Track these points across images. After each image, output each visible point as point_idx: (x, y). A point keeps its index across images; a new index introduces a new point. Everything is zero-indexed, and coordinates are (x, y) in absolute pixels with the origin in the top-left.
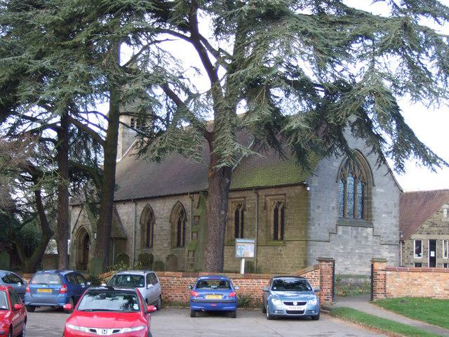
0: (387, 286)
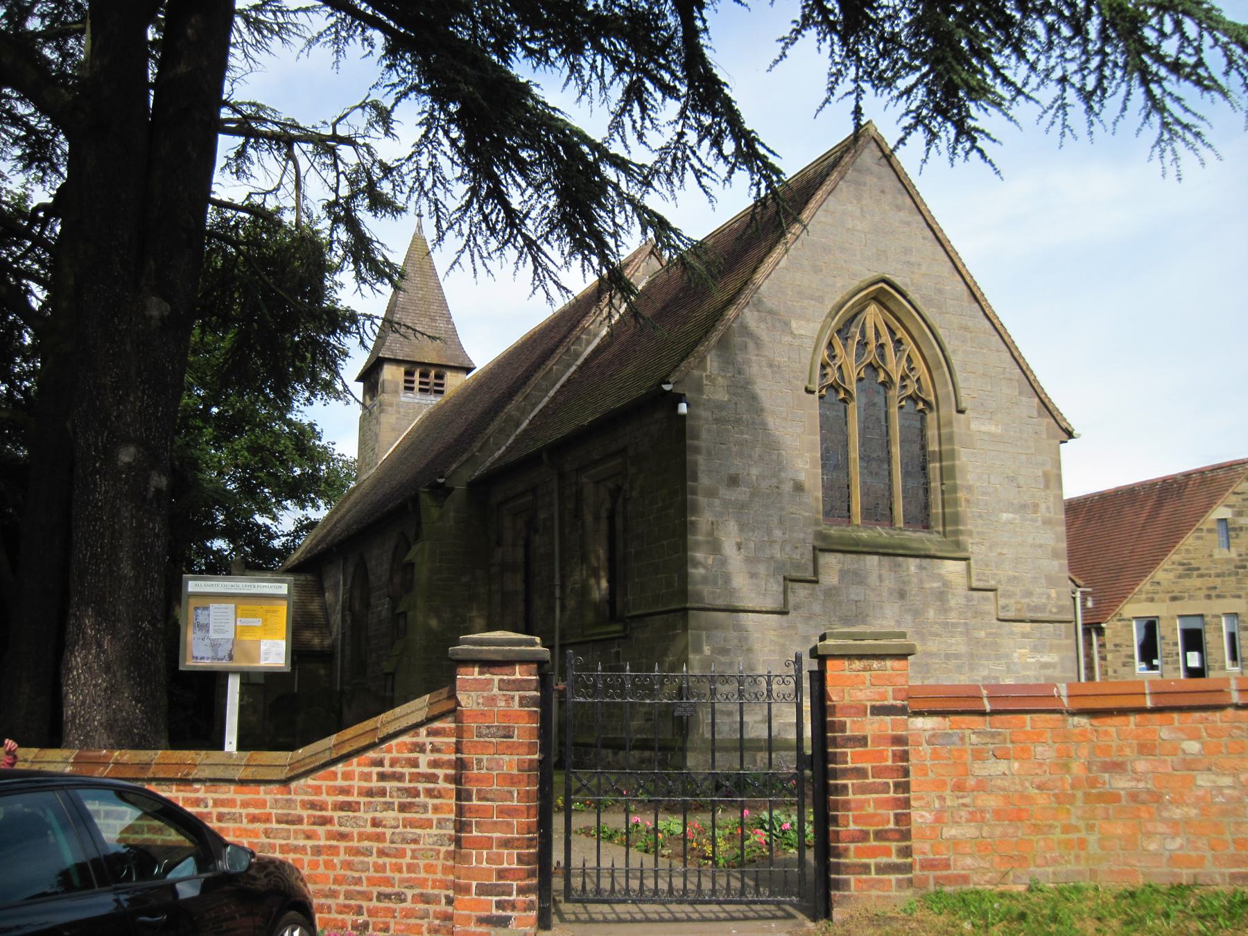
0: (920, 816)
